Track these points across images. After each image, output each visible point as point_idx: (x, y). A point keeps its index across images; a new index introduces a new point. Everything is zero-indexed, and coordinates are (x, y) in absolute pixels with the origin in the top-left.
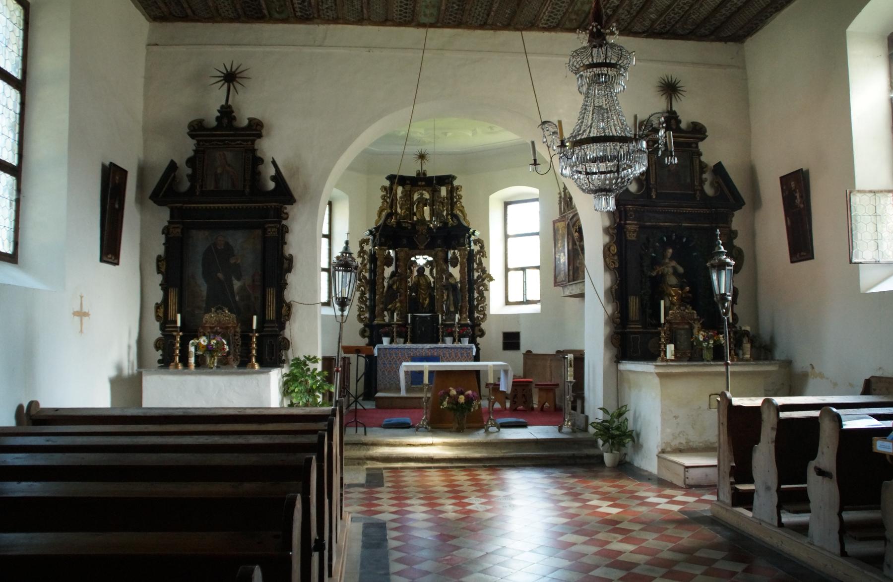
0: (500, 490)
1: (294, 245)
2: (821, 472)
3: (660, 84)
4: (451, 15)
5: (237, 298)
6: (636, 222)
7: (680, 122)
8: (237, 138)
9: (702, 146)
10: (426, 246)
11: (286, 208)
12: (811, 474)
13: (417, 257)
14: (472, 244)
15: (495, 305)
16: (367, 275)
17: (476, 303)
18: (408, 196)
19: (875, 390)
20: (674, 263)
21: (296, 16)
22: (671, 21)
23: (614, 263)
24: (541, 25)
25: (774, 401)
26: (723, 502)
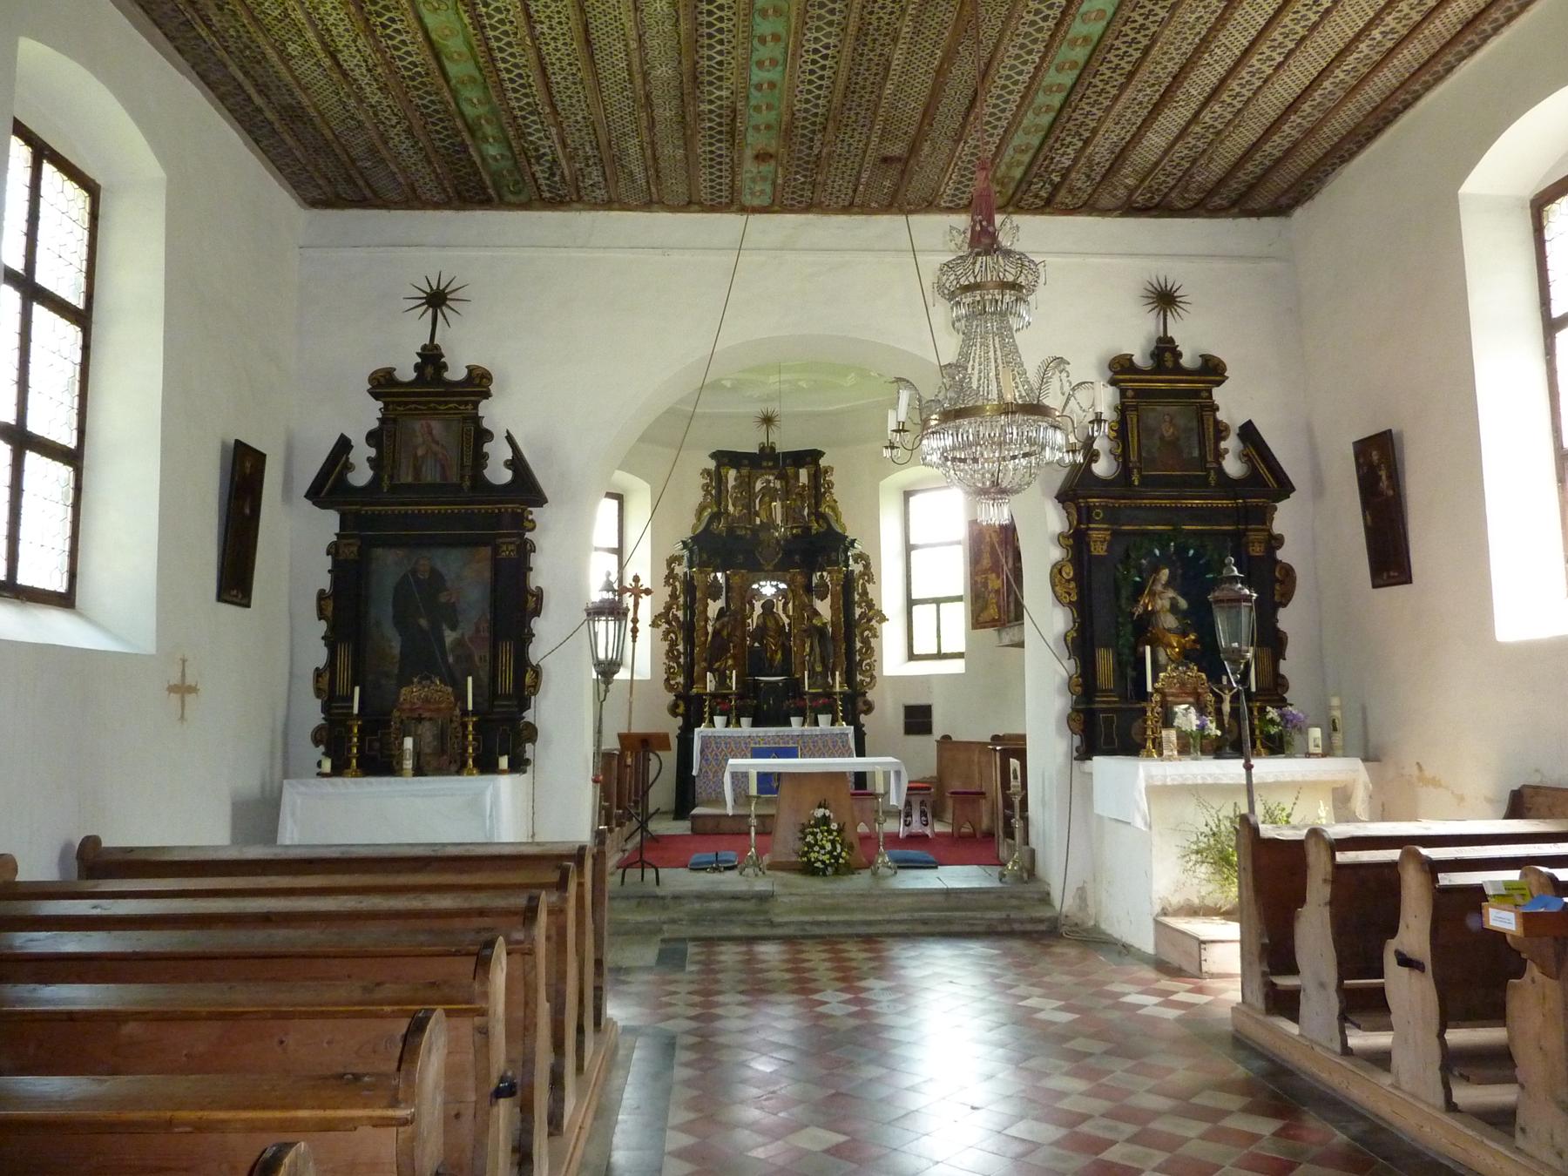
0: (876, 978)
1: (544, 572)
2: (1405, 961)
3: (1145, 293)
4: (793, 193)
5: (451, 659)
6: (1105, 526)
7: (1180, 355)
8: (448, 399)
9: (1219, 395)
10: (775, 566)
11: (531, 513)
12: (1390, 961)
13: (762, 583)
14: (851, 562)
15: (891, 660)
16: (680, 614)
17: (858, 658)
18: (745, 484)
19: (1529, 809)
20: (1171, 594)
21: (542, 199)
22: (1162, 187)
23: (1070, 595)
24: (943, 204)
25: (1325, 834)
26: (1250, 1006)
